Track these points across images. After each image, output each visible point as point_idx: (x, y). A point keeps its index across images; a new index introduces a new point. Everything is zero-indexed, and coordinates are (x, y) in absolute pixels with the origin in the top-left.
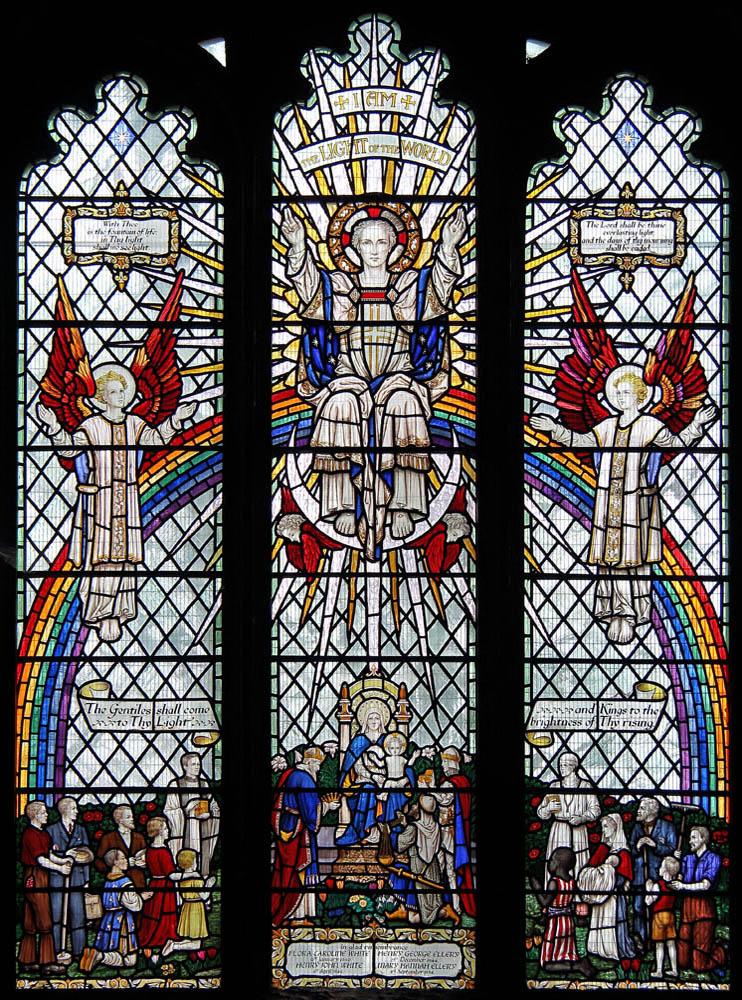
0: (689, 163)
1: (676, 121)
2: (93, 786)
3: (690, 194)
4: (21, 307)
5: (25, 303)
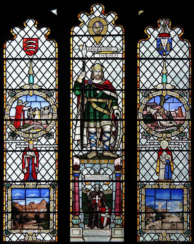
0: (47, 40)
1: (43, 29)
2: (77, 34)
3: (48, 61)
4: (4, 55)
5: (5, 54)
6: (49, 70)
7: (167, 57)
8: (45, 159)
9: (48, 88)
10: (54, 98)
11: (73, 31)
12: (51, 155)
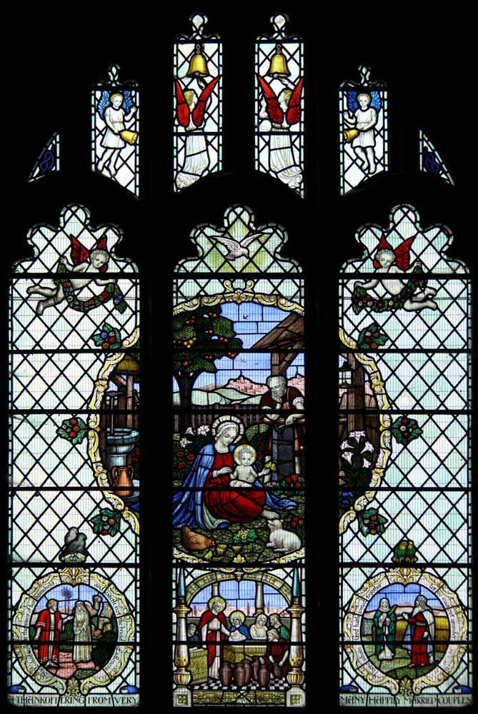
6: (408, 506)
7: (42, 569)
8: (400, 380)
9: (356, 561)
10: (18, 672)
11: (182, 265)
12: (113, 552)
